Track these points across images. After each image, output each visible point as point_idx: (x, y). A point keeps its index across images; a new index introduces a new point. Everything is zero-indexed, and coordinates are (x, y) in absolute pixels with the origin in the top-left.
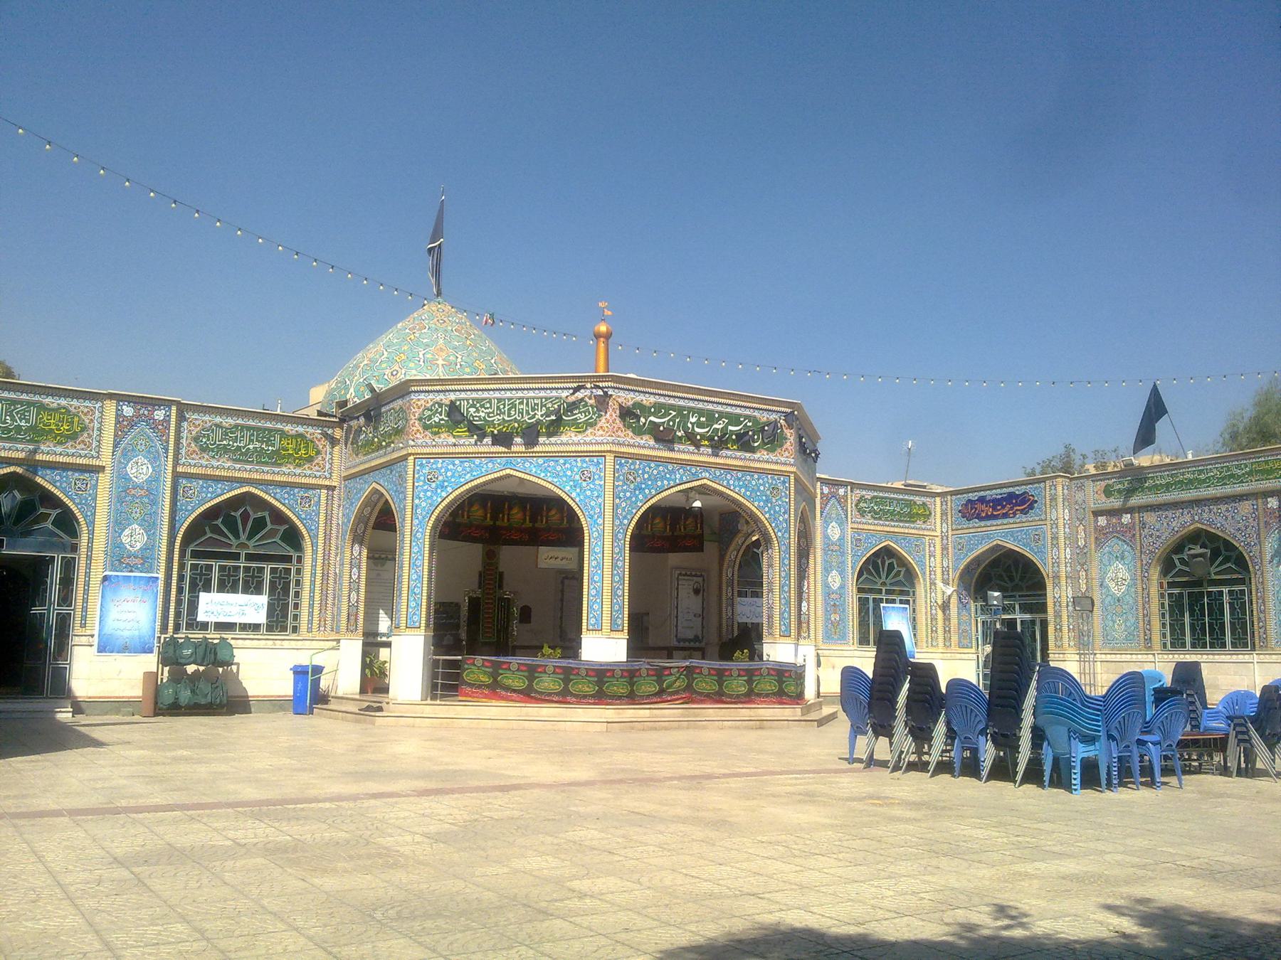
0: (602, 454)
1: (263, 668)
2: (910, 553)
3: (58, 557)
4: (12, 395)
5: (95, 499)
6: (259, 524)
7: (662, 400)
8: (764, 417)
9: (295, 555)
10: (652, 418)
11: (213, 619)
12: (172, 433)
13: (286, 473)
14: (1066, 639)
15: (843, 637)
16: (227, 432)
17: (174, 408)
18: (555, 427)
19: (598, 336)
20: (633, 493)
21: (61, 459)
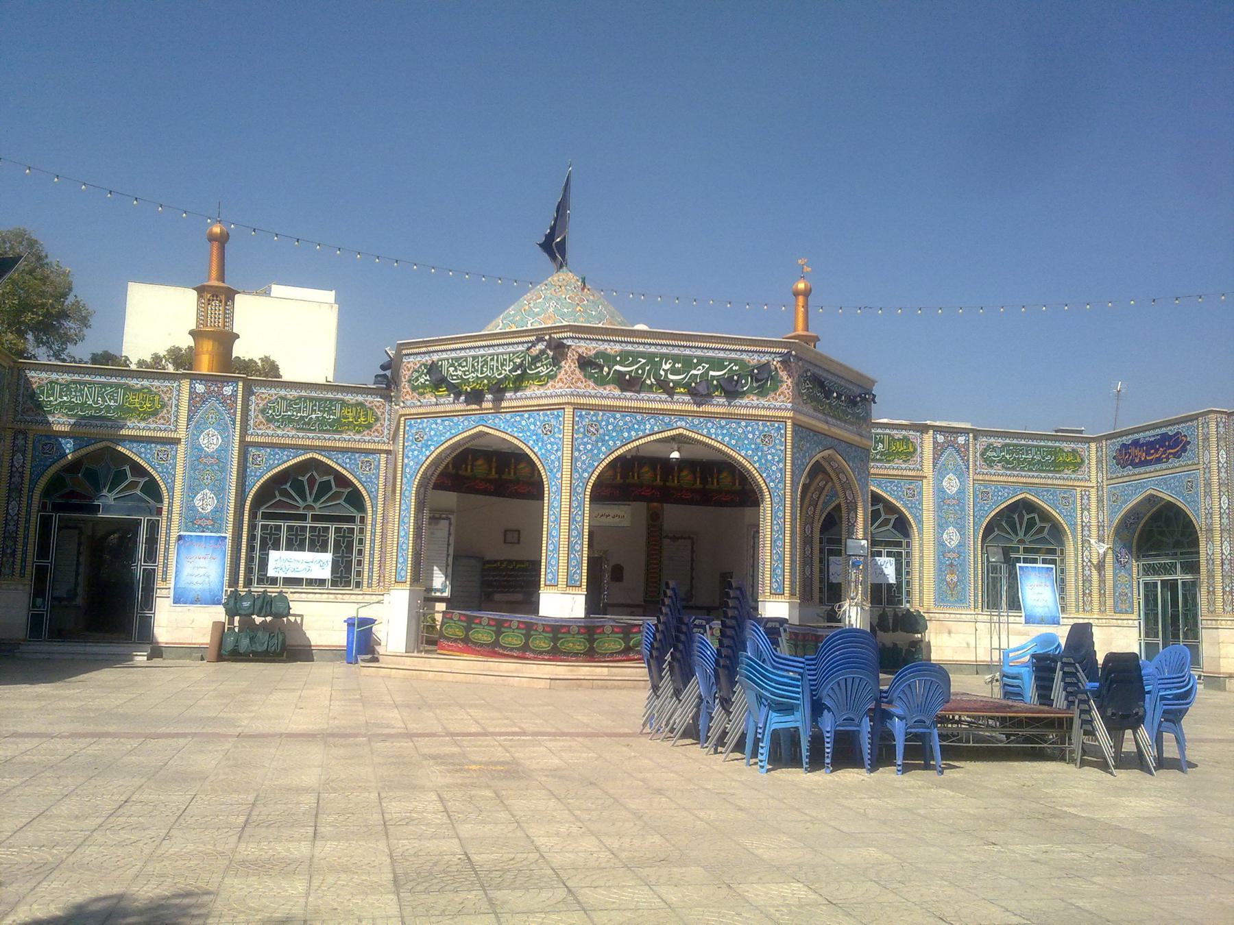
0: (561, 407)
1: (322, 619)
2: (899, 498)
3: (144, 520)
4: (103, 379)
5: (174, 468)
6: (325, 487)
7: (629, 348)
8: (754, 360)
9: (904, 541)
10: (618, 367)
11: (282, 575)
12: (239, 406)
13: (348, 439)
14: (1219, 604)
15: (961, 601)
16: (290, 403)
17: (241, 384)
18: (519, 382)
19: (796, 294)
20: (595, 445)
21: (144, 433)
